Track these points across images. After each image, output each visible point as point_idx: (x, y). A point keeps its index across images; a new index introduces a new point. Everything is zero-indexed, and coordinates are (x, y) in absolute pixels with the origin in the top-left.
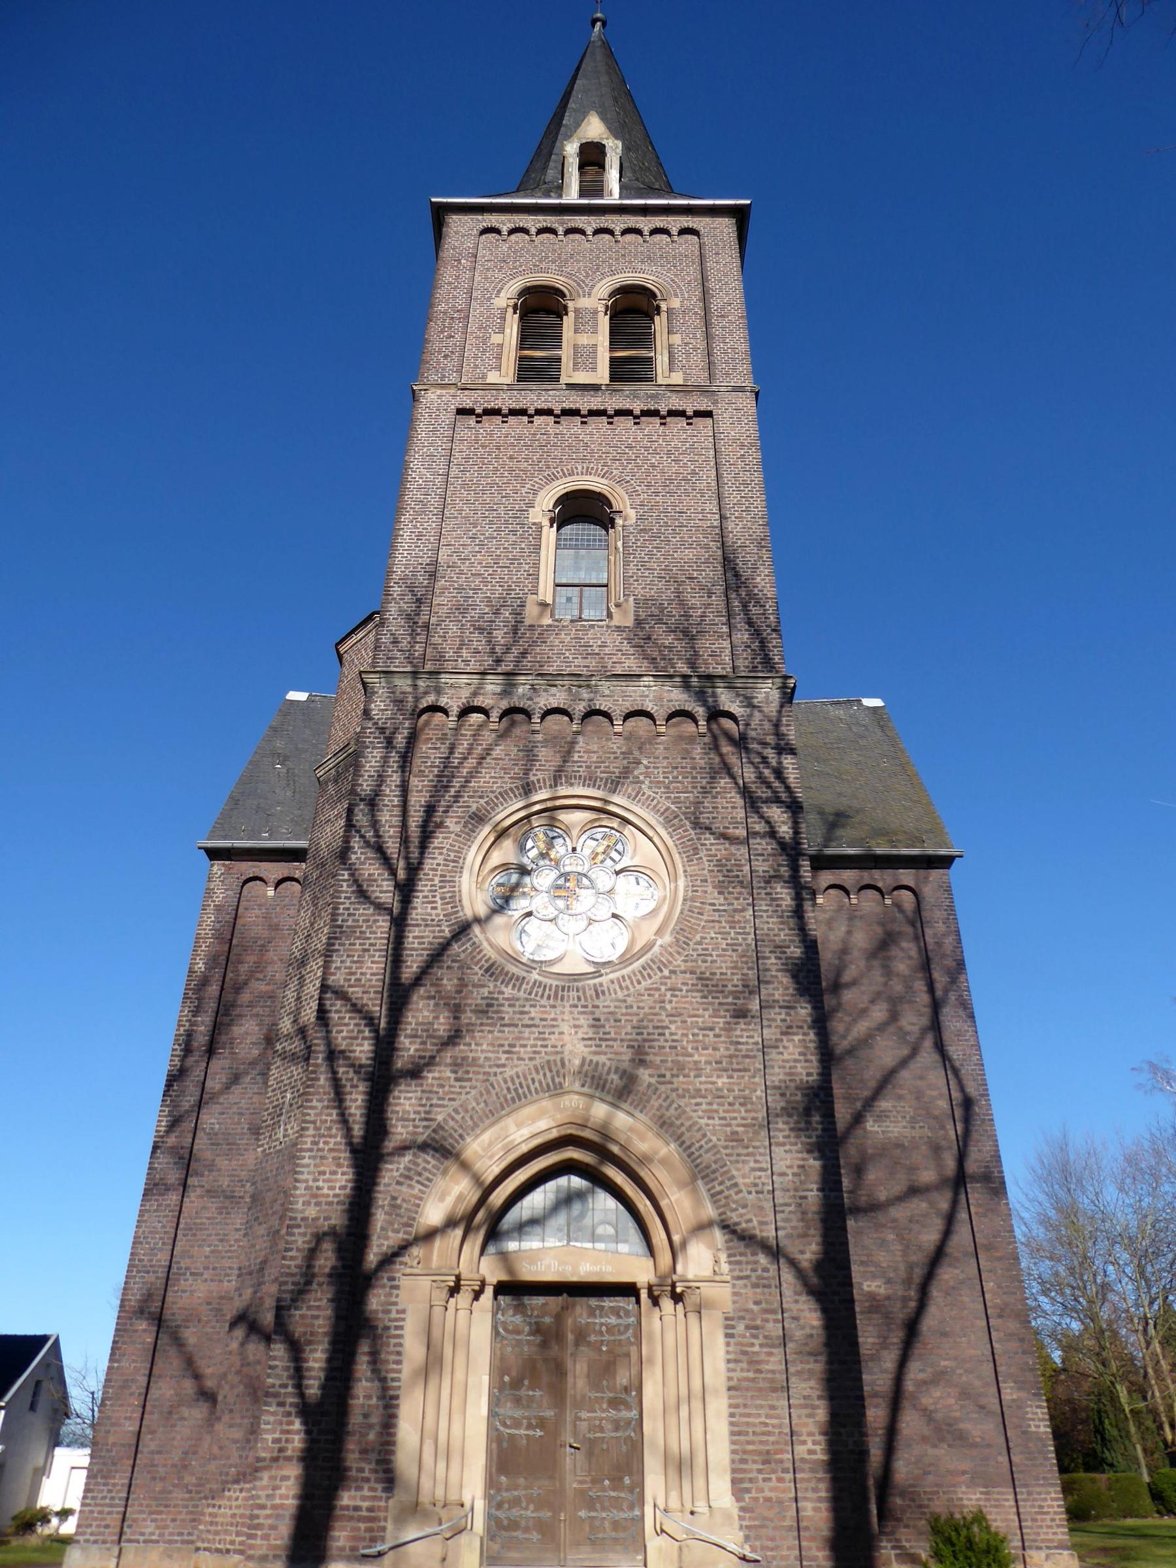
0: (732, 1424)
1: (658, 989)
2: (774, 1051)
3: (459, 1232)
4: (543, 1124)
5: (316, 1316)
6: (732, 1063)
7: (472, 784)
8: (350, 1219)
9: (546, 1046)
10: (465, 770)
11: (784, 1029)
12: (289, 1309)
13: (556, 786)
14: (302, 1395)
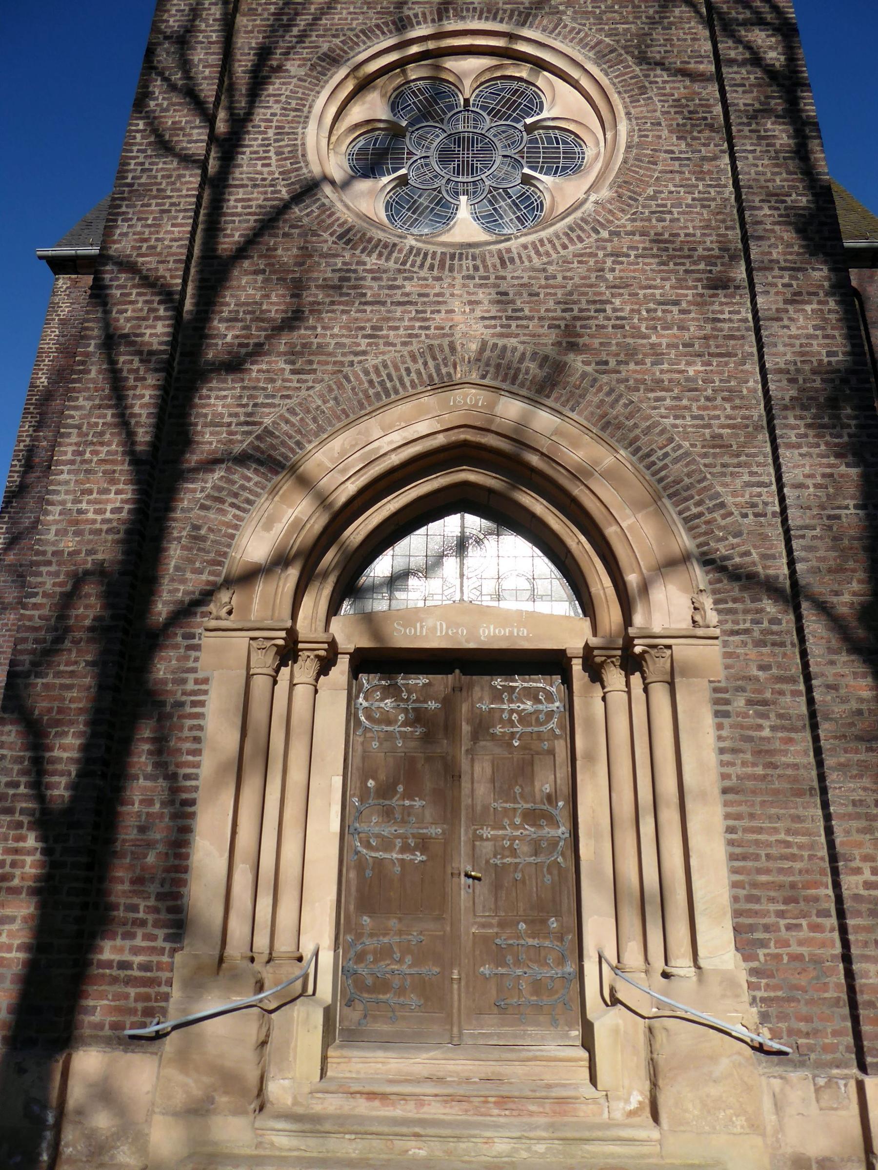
0: (731, 843)
1: (591, 255)
2: (776, 324)
3: (293, 574)
4: (422, 428)
5: (70, 687)
6: (709, 346)
7: (324, 22)
8: (126, 553)
9: (428, 328)
10: (313, 7)
11: (789, 296)
12: (27, 674)
13: (440, 20)
14: (41, 798)
